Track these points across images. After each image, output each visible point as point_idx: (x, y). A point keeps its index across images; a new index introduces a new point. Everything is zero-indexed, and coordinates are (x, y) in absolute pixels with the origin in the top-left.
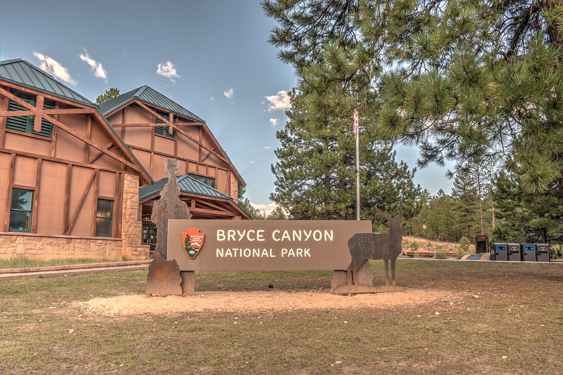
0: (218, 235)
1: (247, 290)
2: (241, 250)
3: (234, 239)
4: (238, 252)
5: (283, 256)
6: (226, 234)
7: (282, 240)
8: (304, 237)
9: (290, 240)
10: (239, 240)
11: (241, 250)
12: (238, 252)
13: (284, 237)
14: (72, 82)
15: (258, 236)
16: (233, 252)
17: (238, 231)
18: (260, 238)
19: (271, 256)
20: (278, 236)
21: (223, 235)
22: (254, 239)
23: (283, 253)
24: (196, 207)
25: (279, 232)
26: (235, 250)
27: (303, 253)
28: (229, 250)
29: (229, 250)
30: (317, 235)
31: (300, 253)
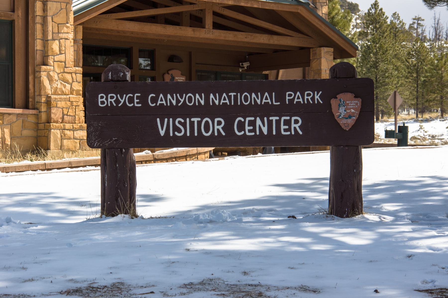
0: (100, 100)
1: (165, 217)
2: (239, 94)
3: (115, 105)
4: (236, 97)
5: (295, 103)
6: (107, 99)
7: (158, 104)
8: (178, 101)
9: (165, 105)
10: (120, 105)
11: (239, 94)
12: (236, 97)
13: (159, 102)
14: (20, 8)
15: (136, 101)
16: (230, 97)
17: (118, 95)
18: (137, 103)
19: (274, 103)
20: (154, 100)
21: (104, 99)
22: (132, 105)
23: (287, 98)
24: (216, 26)
25: (154, 95)
26: (232, 94)
27: (313, 99)
28: (224, 95)
29: (224, 95)
30: (190, 99)
31: (309, 98)
